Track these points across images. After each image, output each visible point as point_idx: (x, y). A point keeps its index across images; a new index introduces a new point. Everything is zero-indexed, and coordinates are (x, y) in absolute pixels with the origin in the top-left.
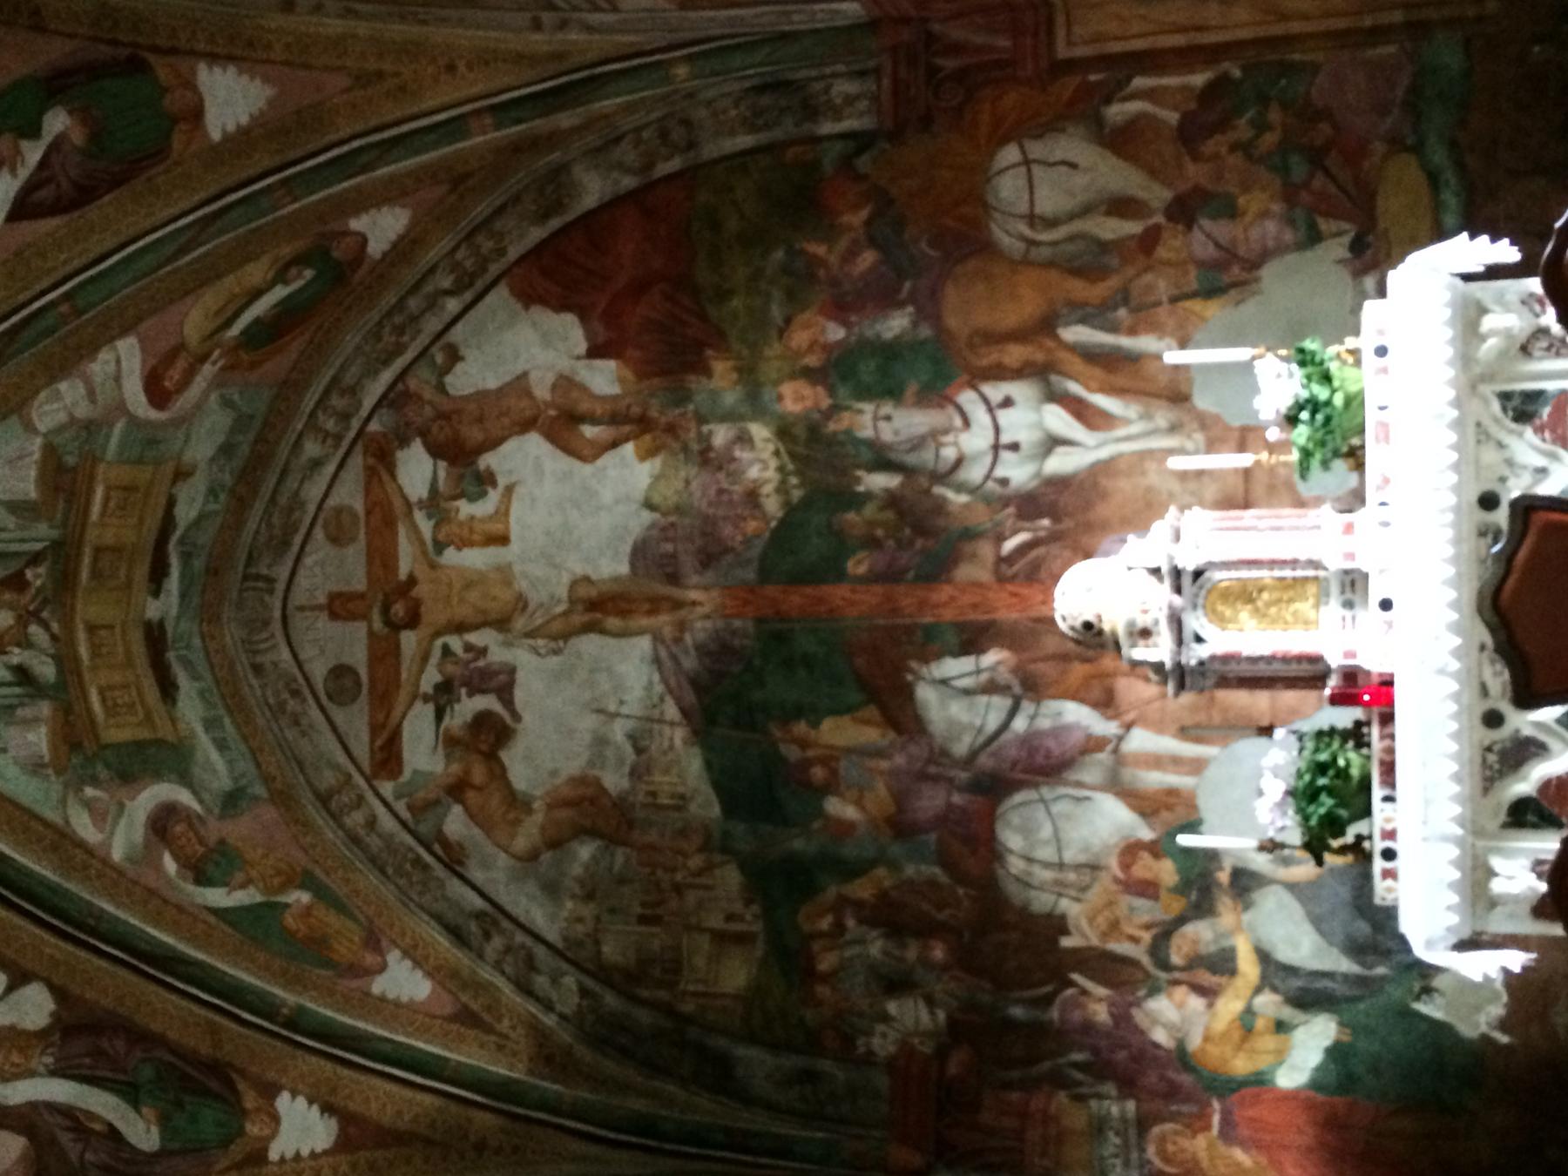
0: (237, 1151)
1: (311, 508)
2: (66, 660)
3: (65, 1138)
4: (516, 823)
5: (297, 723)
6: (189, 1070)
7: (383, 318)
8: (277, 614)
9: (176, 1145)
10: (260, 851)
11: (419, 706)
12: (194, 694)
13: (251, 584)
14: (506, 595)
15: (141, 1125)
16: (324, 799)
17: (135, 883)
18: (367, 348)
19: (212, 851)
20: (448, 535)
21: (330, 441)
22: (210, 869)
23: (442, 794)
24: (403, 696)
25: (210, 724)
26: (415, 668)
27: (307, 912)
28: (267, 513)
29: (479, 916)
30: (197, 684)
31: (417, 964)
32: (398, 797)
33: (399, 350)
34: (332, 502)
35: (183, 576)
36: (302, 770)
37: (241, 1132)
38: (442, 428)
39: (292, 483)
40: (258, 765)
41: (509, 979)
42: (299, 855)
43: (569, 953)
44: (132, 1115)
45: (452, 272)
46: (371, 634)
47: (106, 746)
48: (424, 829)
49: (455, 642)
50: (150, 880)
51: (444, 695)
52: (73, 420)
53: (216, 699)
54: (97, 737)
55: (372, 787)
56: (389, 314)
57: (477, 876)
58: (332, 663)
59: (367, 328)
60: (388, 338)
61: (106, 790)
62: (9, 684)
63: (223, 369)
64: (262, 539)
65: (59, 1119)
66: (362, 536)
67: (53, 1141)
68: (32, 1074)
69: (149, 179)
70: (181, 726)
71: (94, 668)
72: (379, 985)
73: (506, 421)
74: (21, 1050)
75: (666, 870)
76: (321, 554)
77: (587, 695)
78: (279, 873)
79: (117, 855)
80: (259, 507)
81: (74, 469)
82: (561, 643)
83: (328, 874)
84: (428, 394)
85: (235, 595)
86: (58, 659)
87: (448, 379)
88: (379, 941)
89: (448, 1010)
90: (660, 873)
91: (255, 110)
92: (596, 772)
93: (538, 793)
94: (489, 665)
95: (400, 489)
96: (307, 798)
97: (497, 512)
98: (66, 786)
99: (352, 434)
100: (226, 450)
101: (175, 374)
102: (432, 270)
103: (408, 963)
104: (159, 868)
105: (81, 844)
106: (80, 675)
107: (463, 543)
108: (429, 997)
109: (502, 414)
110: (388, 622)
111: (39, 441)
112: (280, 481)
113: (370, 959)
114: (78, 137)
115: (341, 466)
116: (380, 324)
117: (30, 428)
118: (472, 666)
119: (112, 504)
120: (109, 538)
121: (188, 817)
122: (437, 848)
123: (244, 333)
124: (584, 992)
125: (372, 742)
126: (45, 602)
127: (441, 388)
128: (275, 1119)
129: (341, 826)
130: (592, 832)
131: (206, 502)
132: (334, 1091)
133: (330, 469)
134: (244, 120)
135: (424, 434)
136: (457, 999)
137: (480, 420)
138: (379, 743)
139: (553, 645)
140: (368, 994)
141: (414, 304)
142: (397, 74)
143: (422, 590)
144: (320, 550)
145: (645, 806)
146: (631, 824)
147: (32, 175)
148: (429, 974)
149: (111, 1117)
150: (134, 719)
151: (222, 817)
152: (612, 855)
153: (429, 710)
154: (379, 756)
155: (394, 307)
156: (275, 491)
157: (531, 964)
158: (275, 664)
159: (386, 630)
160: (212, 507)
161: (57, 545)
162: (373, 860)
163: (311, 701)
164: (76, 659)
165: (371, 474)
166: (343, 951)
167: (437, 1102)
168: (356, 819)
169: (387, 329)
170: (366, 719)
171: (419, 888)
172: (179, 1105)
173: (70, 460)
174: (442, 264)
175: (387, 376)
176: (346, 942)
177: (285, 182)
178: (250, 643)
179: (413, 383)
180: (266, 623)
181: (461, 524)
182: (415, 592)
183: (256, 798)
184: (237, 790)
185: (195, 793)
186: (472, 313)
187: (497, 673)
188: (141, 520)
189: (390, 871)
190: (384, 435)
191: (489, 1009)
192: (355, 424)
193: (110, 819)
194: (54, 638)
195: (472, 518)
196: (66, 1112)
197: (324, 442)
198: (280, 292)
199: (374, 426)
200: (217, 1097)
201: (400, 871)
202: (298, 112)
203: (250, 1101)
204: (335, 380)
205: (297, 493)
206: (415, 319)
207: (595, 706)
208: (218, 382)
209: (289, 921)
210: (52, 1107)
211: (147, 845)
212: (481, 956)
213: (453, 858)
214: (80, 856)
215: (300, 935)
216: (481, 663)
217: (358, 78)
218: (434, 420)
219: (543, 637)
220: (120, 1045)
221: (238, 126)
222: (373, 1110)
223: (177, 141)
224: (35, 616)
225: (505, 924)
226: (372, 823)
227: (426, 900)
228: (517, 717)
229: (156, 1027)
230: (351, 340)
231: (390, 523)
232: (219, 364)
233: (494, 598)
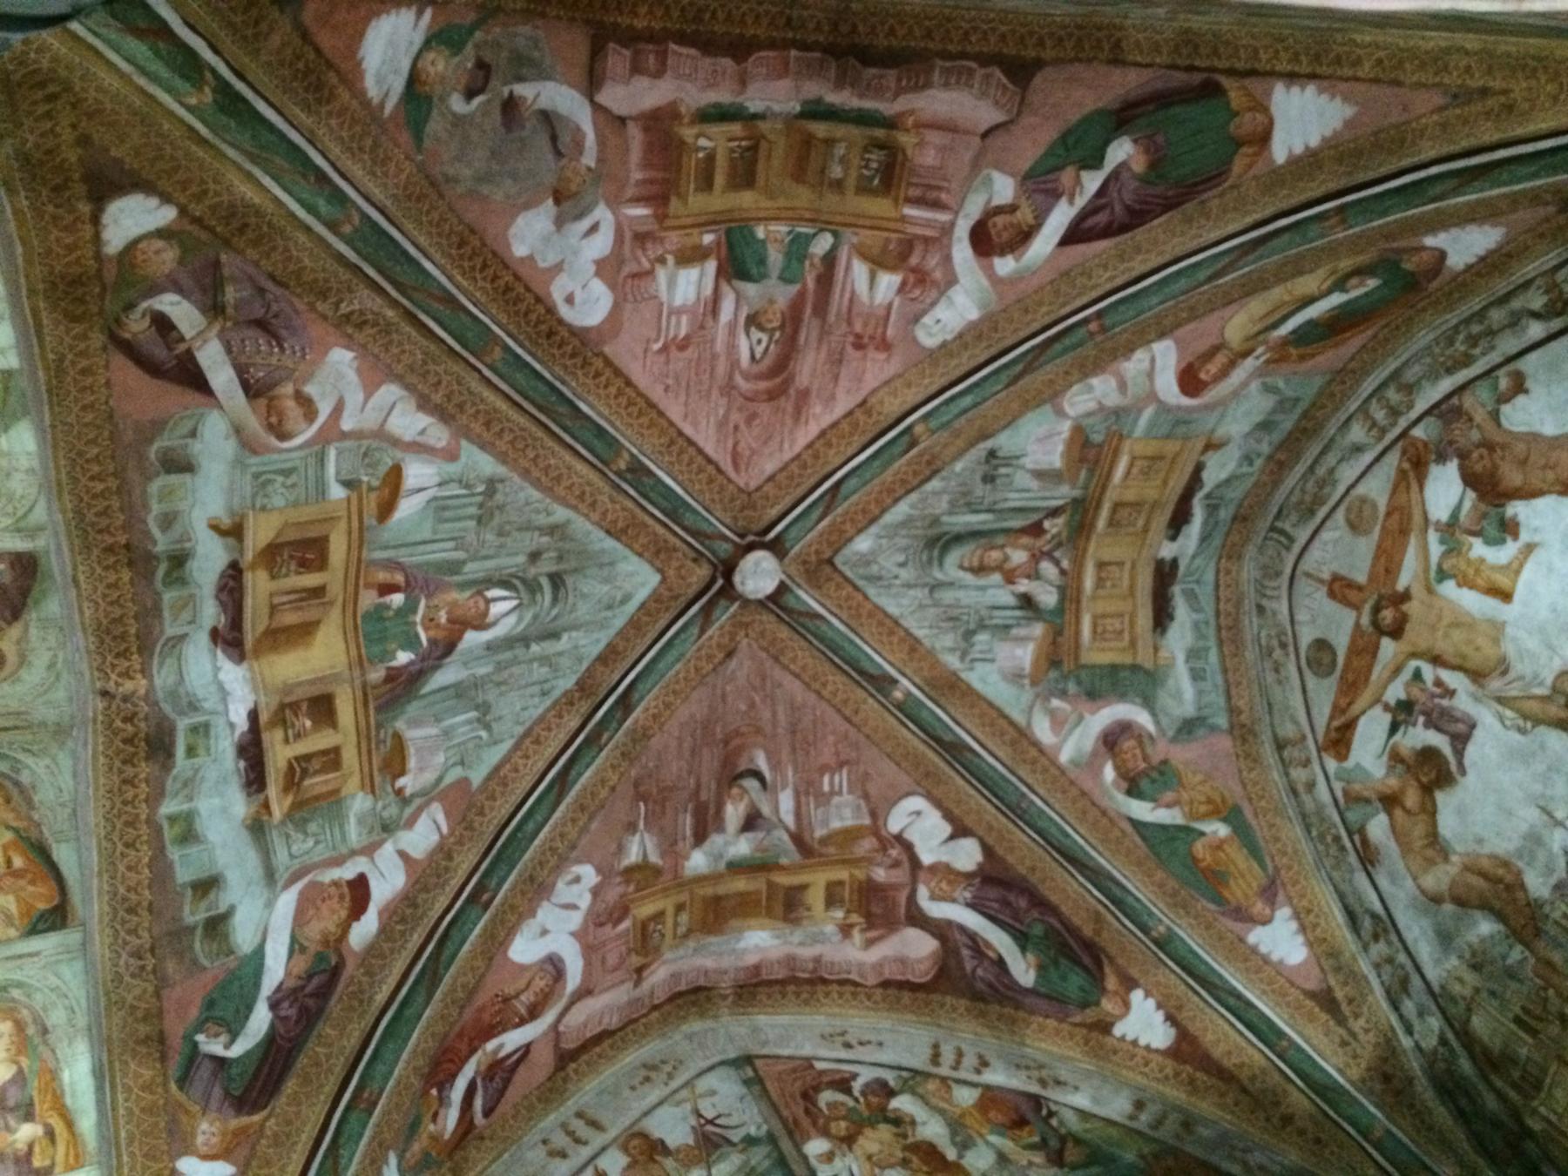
0: (1090, 1015)
1: (1341, 489)
2: (1070, 594)
3: (965, 952)
4: (1431, 862)
5: (1277, 671)
6: (1071, 941)
7: (1461, 323)
8: (1288, 571)
9: (1043, 990)
10: (1199, 777)
11: (1377, 711)
12: (1188, 625)
13: (1275, 536)
14: (1489, 651)
15: (1023, 966)
16: (1280, 745)
17: (1072, 783)
18: (1437, 350)
19: (1153, 768)
20: (1454, 566)
21: (1374, 432)
22: (1145, 784)
23: (1374, 797)
24: (1366, 696)
25: (1193, 654)
26: (1386, 674)
27: (1219, 846)
28: (1304, 478)
29: (1374, 916)
30: (1195, 616)
31: (1303, 929)
32: (1339, 778)
33: (1467, 361)
34: (1361, 490)
35: (1205, 523)
36: (1270, 713)
37: (1097, 1004)
38: (1482, 457)
39: (1331, 459)
40: (1229, 697)
41: (1382, 983)
42: (1238, 789)
43: (1440, 998)
44: (1019, 955)
45: (1547, 292)
46: (1357, 625)
47: (1084, 667)
48: (1351, 816)
49: (1428, 672)
50: (1088, 785)
51: (1403, 712)
52: (1102, 407)
53: (1211, 632)
54: (1077, 658)
55: (1320, 758)
56: (1467, 321)
57: (1383, 882)
58: (1318, 634)
59: (1444, 328)
60: (1460, 347)
61: (1069, 702)
62: (1013, 608)
63: (1268, 362)
64: (1294, 499)
65: (965, 939)
66: (1377, 529)
67: (957, 953)
68: (954, 901)
69: (1203, 202)
70: (1163, 654)
71: (1094, 598)
72: (1258, 936)
73: (1550, 475)
74: (950, 882)
75: (1559, 994)
76: (1337, 534)
77: (1538, 788)
78: (1209, 801)
79: (1064, 757)
80: (1300, 469)
81: (1100, 446)
82: (1529, 725)
83: (1256, 815)
84: (1480, 416)
85: (1259, 541)
86: (1062, 590)
87: (1506, 409)
88: (1275, 895)
89: (1312, 985)
90: (1551, 992)
91: (1328, 133)
92: (1520, 864)
93: (1459, 848)
94: (1453, 708)
95: (1423, 503)
96: (1266, 737)
97: (1510, 564)
98: (1037, 696)
99: (1397, 431)
100: (1265, 426)
101: (1213, 367)
102: (1526, 285)
103: (1294, 925)
104: (1097, 773)
105: (1036, 744)
106: (1078, 602)
107: (1465, 582)
108: (1300, 965)
109: (1545, 467)
110: (1375, 623)
111: (1066, 427)
112: (1323, 453)
113: (1259, 907)
114: (1139, 166)
115: (1377, 459)
116: (1456, 329)
117: (1060, 413)
118: (1437, 700)
119: (1135, 470)
120: (1130, 495)
121: (1140, 736)
122: (1356, 838)
123: (1294, 332)
124: (1443, 1041)
125: (1332, 718)
126: (1060, 545)
127: (1495, 416)
128: (1127, 1005)
129: (1287, 774)
130: (1500, 916)
131: (1240, 465)
132: (1180, 1008)
133: (1368, 457)
134: (1314, 142)
135: (1463, 456)
136: (1325, 980)
137: (1523, 463)
138: (1336, 723)
139: (1521, 722)
140: (1242, 940)
141: (1497, 316)
142: (1505, 92)
143: (1413, 608)
144: (1336, 531)
145: (1556, 922)
146: (1538, 933)
147: (1090, 202)
148: (1310, 944)
150: (1120, 645)
151: (1174, 740)
152: (1511, 947)
153: (1387, 718)
154: (1333, 735)
155: (1473, 315)
156: (1316, 462)
157: (1404, 983)
158: (1274, 614)
159: (1371, 629)
160: (1245, 469)
161: (1076, 502)
162: (1304, 816)
163: (1292, 656)
164: (1079, 590)
165: (1402, 475)
166: (1239, 894)
167: (1263, 1062)
168: (1299, 774)
169: (1461, 337)
170: (1332, 697)
171: (1333, 861)
172: (1056, 963)
173: (1097, 438)
174: (1537, 282)
175: (1446, 384)
176: (1245, 879)
177: (1341, 209)
178: (1264, 587)
179: (1468, 401)
180: (1278, 574)
181: (1469, 562)
182: (1405, 607)
183: (1213, 729)
184: (1198, 719)
185: (1154, 714)
186: (1554, 345)
187: (1457, 720)
188: (1165, 483)
189: (1314, 833)
190: (1425, 444)
191: (1350, 1001)
192: (1403, 423)
193: (1067, 727)
194: (1063, 572)
195: (1482, 560)
196: (973, 938)
197: (1370, 430)
198: (1337, 299)
199: (1418, 432)
200: (1086, 969)
201: (1322, 837)
202: (1375, 134)
203: (1111, 982)
204: (1396, 375)
205: (1332, 471)
206: (1491, 333)
207: (1542, 803)
208: (1259, 373)
209: (1199, 848)
210: (962, 929)
211: (1095, 754)
212: (1366, 948)
213: (1368, 857)
214: (1033, 752)
215: (1203, 864)
216: (1445, 702)
217: (1455, 96)
218: (1478, 446)
219: (1512, 709)
220: (1023, 903)
221: (1307, 148)
222: (1208, 1039)
223: (1238, 165)
224: (1049, 555)
225: (1394, 938)
226: (1311, 786)
227: (1335, 874)
228: (1463, 770)
229: (1054, 898)
230: (1423, 337)
231: (1404, 532)
232: (1263, 359)
233: (1477, 649)
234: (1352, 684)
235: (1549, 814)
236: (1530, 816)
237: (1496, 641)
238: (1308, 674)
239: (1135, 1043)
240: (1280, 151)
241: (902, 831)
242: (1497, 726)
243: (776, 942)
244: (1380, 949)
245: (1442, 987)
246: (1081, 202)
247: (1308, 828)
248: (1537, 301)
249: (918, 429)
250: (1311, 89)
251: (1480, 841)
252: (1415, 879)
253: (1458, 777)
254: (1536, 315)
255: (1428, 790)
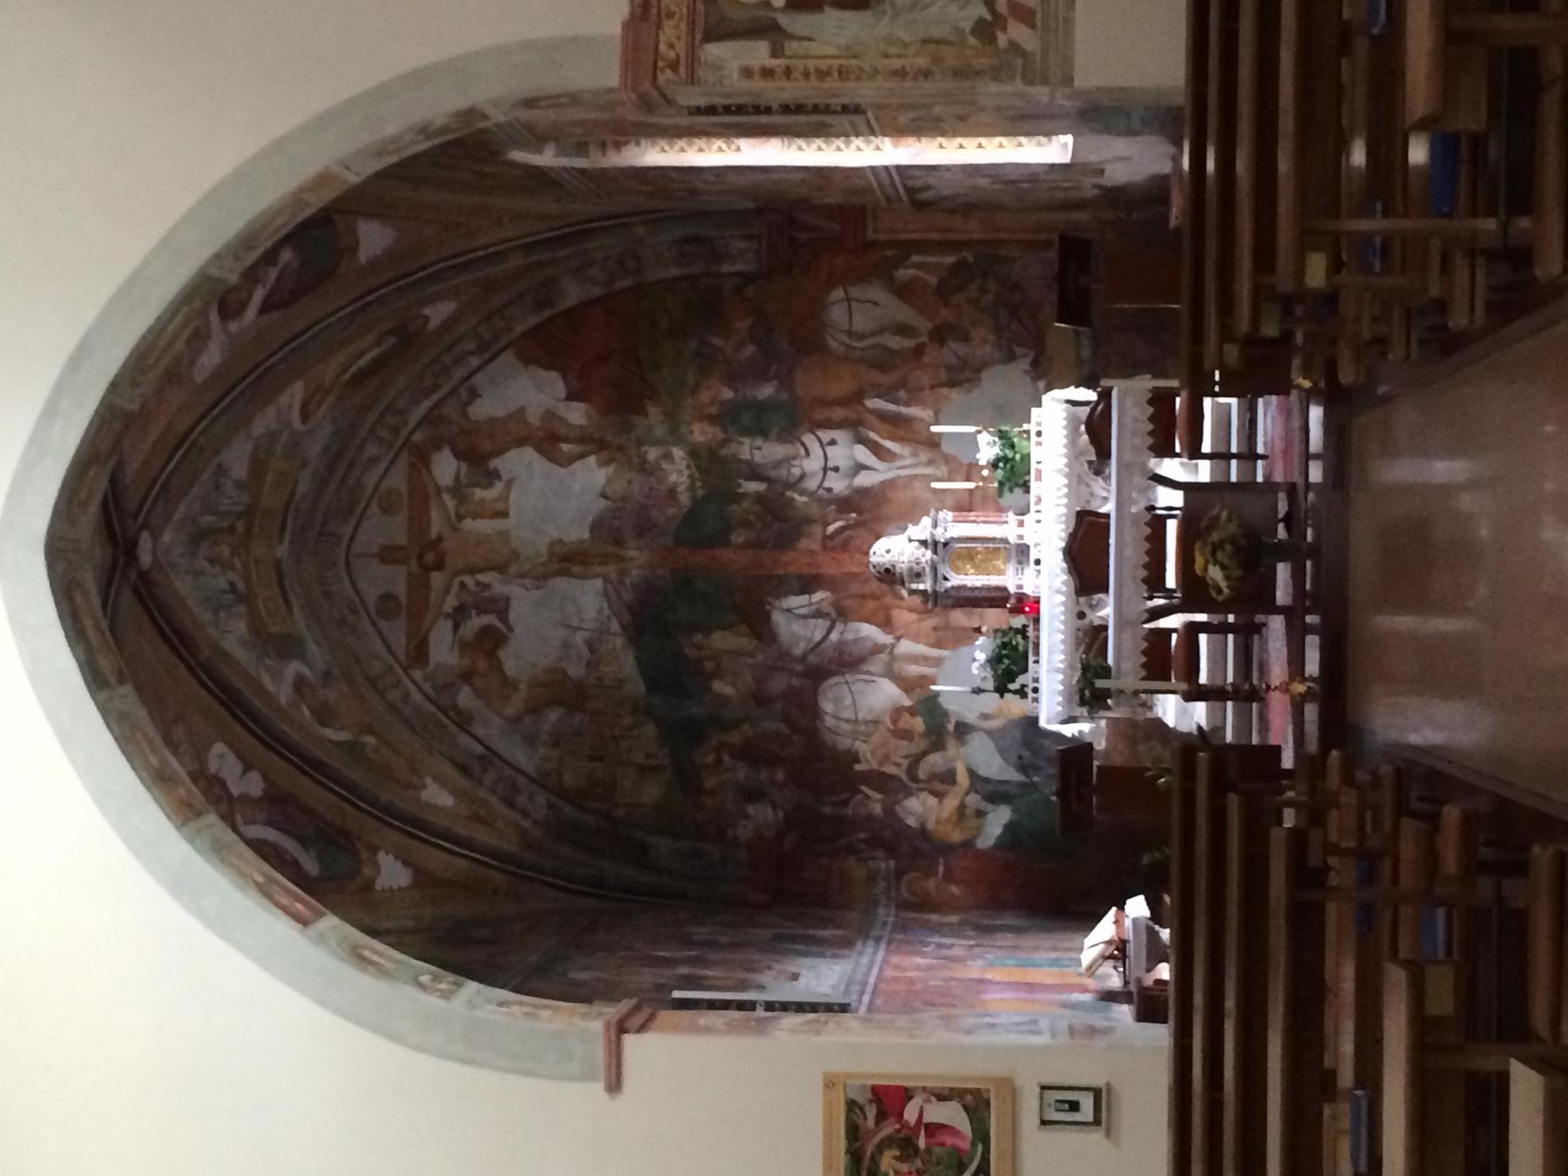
8: (342, 560)
33: (436, 388)
34: (385, 485)
43: (539, 781)
46: (410, 574)
51: (459, 615)
87: (470, 409)
102: (461, 339)
107: (476, 516)
115: (392, 462)
122: (452, 714)
125: (408, 642)
127: (465, 415)
128: (377, 866)
133: (383, 465)
141: (447, 359)
143: (448, 544)
149: (296, 855)
153: (449, 623)
156: (346, 475)
157: (515, 788)
162: (406, 721)
163: (364, 616)
165: (412, 466)
168: (394, 695)
175: (427, 404)
192: (403, 434)
203: (364, 854)
204: (389, 408)
216: (486, 594)
225: (497, 761)
226: (406, 697)
228: (510, 629)
235: (569, 627)
236: (558, 634)
238: (382, 624)
239: (391, 889)
240: (363, 256)
241: (217, 772)
244: (490, 776)
247: (413, 729)
248: (471, 346)
249: (202, 440)
251: (534, 665)
252: (499, 715)
253: (508, 634)
254: (471, 353)
255: (492, 655)
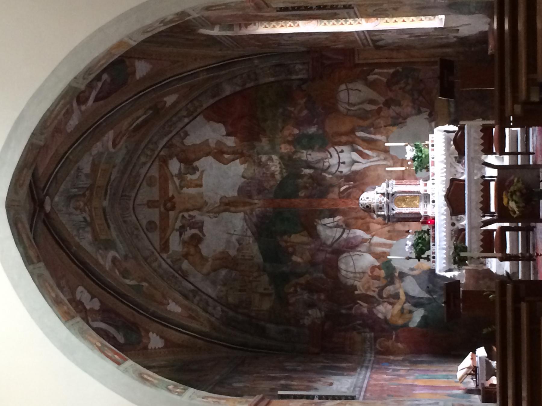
1: (142, 176)
8: (131, 206)
16: (146, 259)
29: (192, 291)
33: (170, 132)
43: (218, 300)
46: (160, 211)
49: (186, 215)
51: (182, 230)
82: (217, 215)
87: (185, 141)
92: (227, 250)
99: (155, 156)
102: (180, 110)
103: (174, 303)
105: (100, 264)
111: (91, 158)
114: (109, 80)
115: (152, 164)
118: (191, 221)
122: (179, 272)
127: (183, 143)
128: (149, 338)
129: (151, 267)
130: (226, 267)
133: (148, 165)
134: (145, 74)
135: (177, 156)
139: (215, 215)
140: (166, 310)
141: (174, 119)
157: (207, 303)
165: (160, 166)
168: (155, 265)
175: (166, 139)
179: (174, 141)
189: (165, 279)
192: (156, 153)
195: (191, 180)
199: (162, 153)
203: (143, 334)
212: (193, 302)
216: (193, 220)
226: (160, 266)
231: (166, 180)
234: (164, 229)
235: (230, 234)
237: (202, 198)
240: (138, 75)
241: (80, 299)
242: (209, 218)
243: (245, 166)
245: (218, 297)
246: (98, 90)
249: (71, 157)
250: (143, 61)
254: (185, 117)
255: (196, 246)
